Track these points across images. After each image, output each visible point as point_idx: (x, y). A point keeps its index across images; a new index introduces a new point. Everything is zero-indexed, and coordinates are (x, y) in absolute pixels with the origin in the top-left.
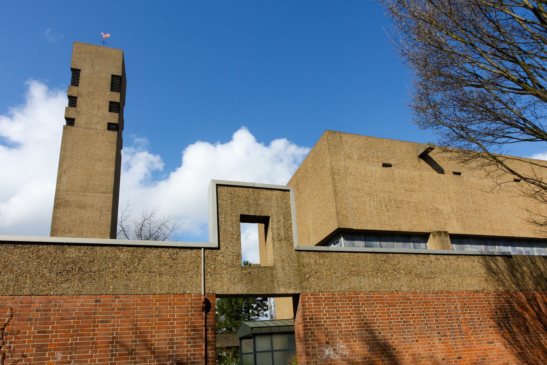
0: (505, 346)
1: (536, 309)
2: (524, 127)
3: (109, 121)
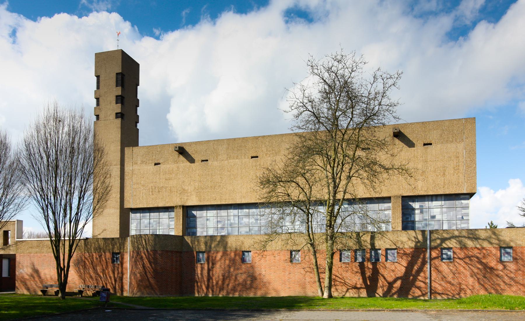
0: (75, 273)
2: (42, 200)
3: (116, 112)
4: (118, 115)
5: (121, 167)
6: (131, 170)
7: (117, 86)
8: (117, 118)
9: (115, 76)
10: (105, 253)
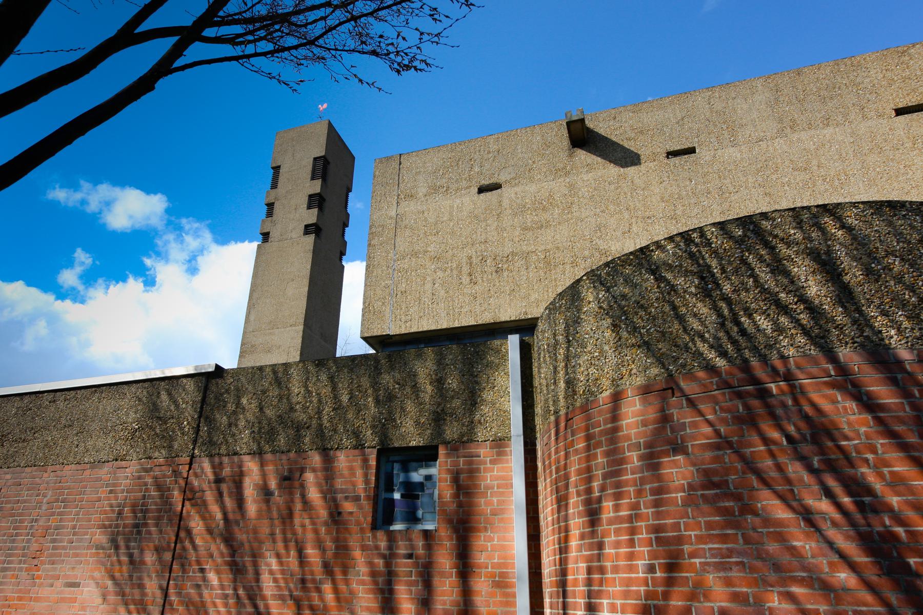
1: (229, 503)
3: (306, 223)
4: (308, 230)
5: (304, 328)
6: (391, 218)
7: (313, 178)
8: (307, 234)
9: (312, 162)
10: (326, 453)
